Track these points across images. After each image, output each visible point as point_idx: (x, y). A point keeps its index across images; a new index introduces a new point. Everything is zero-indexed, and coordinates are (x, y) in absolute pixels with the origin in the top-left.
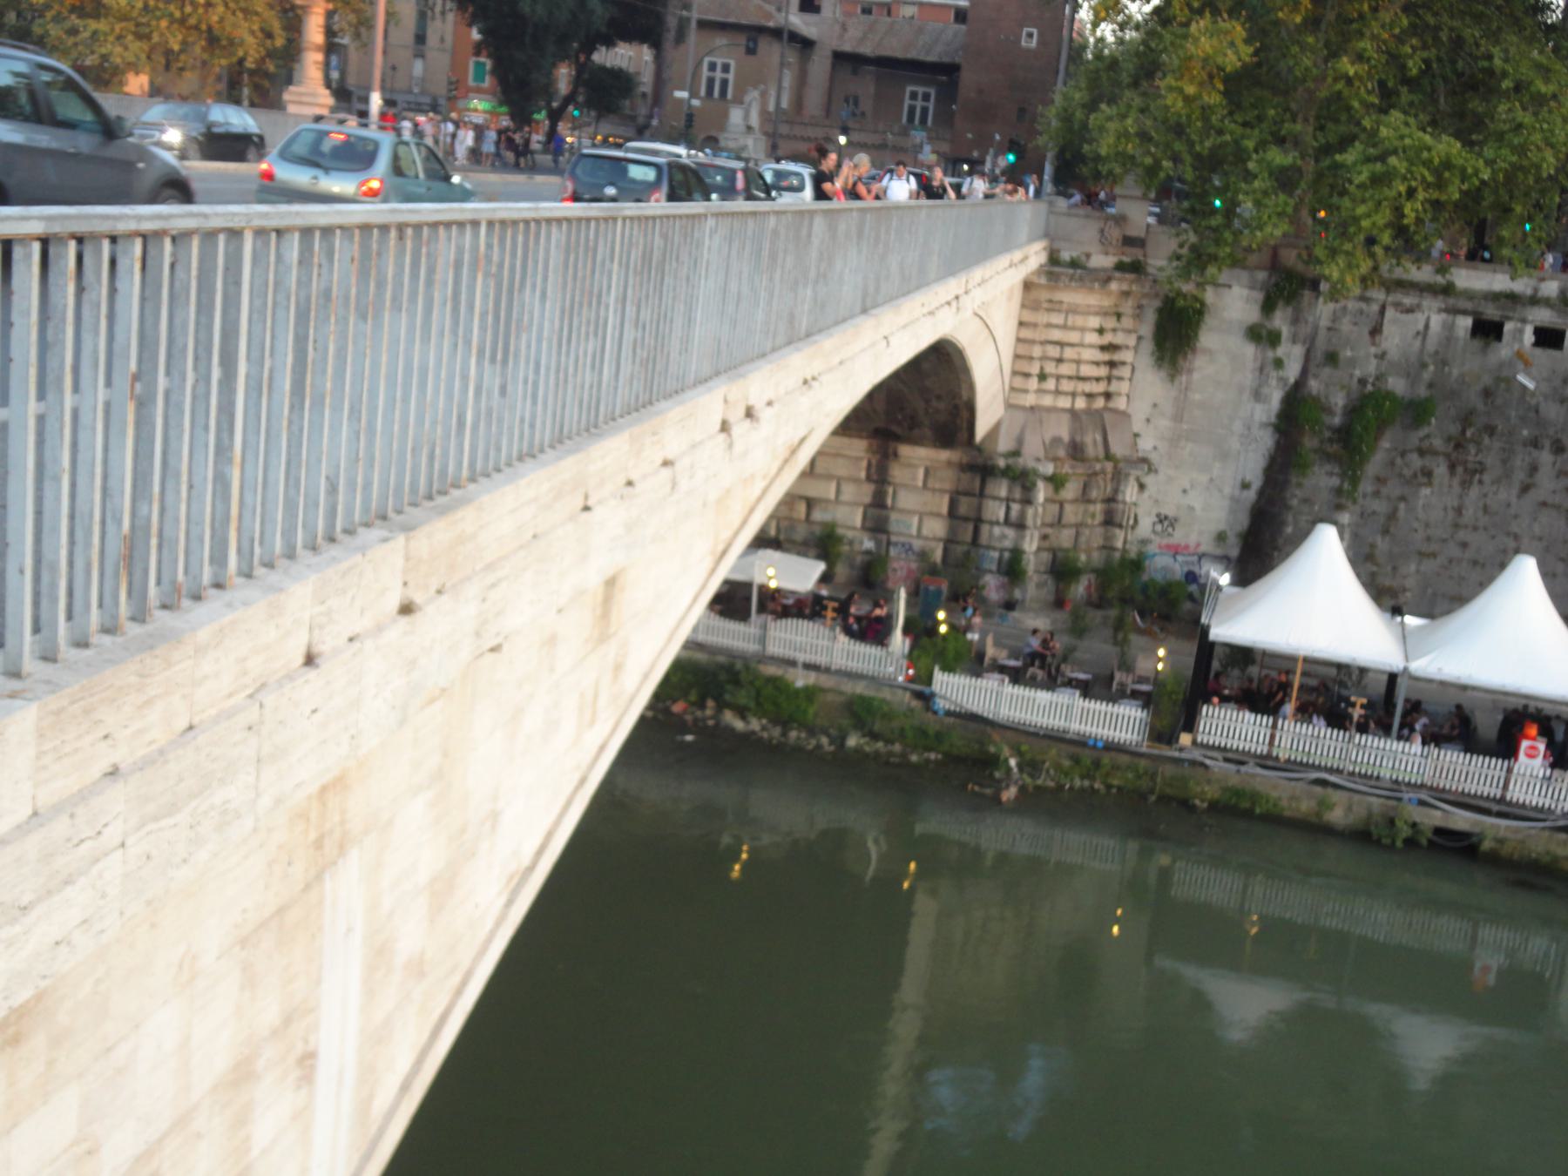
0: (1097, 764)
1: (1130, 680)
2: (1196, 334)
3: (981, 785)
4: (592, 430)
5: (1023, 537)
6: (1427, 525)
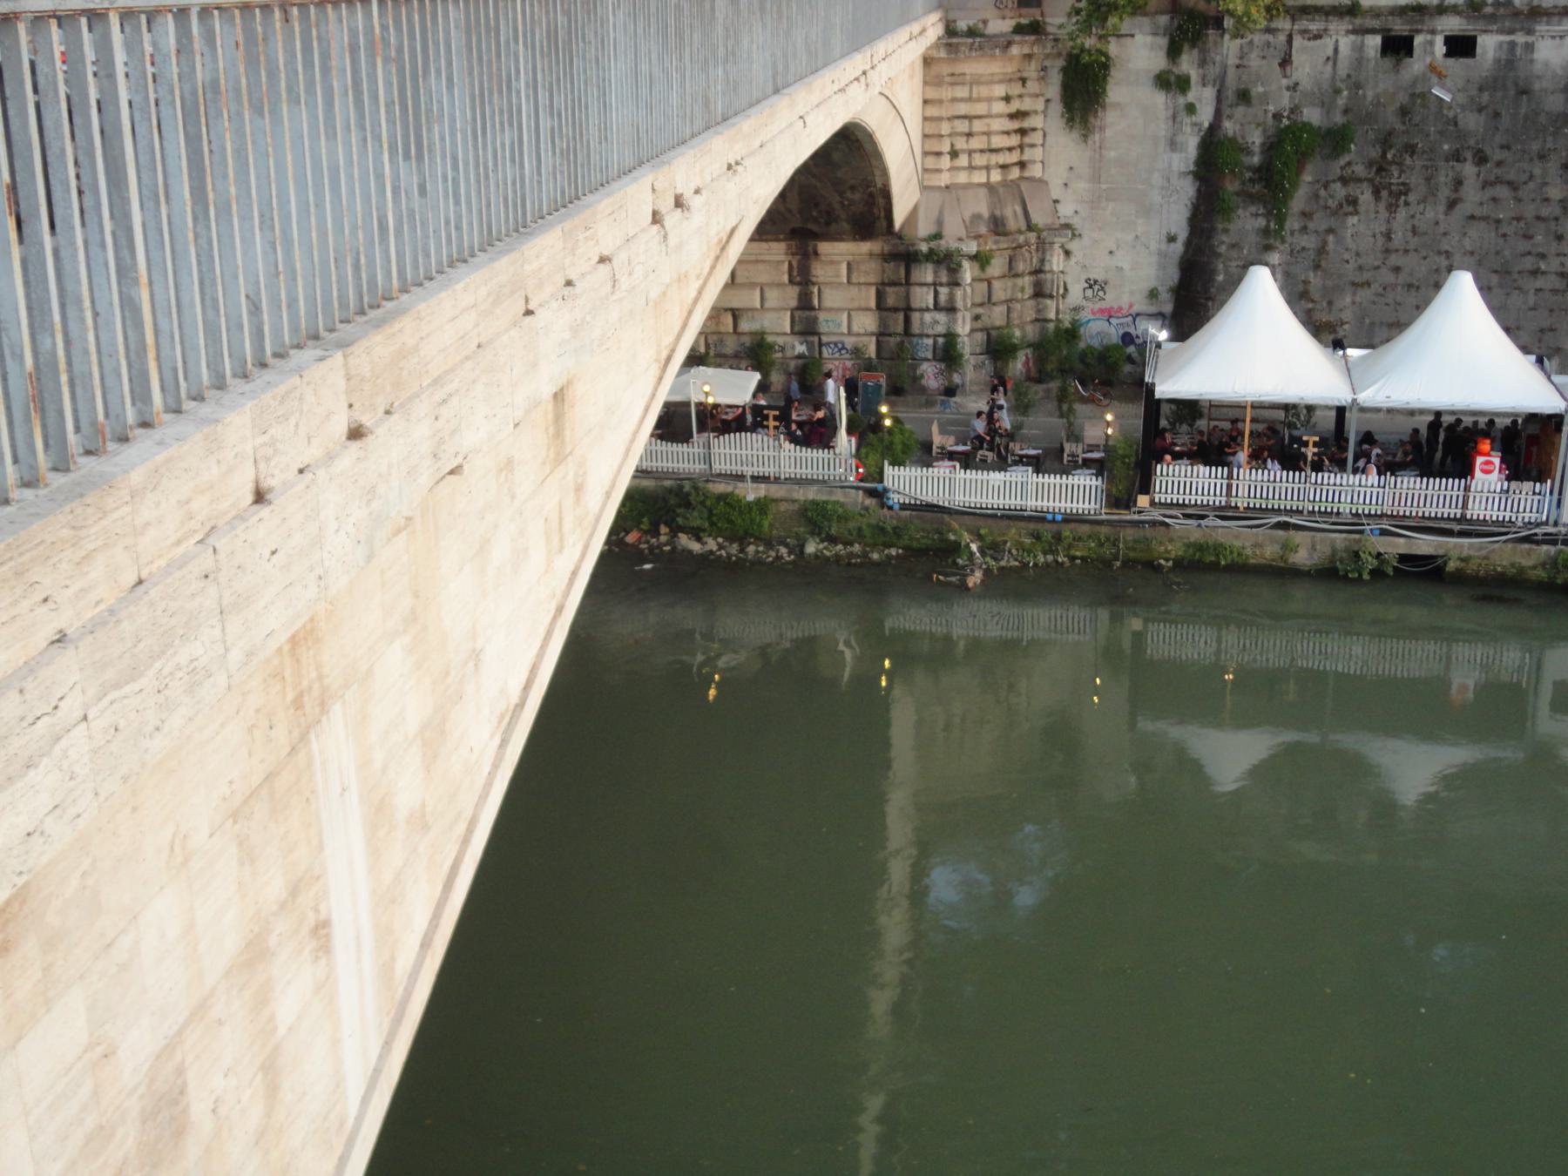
0: (1058, 537)
1: (1080, 450)
2: (1105, 90)
3: (946, 575)
4: (521, 230)
5: (955, 321)
6: (1358, 254)
